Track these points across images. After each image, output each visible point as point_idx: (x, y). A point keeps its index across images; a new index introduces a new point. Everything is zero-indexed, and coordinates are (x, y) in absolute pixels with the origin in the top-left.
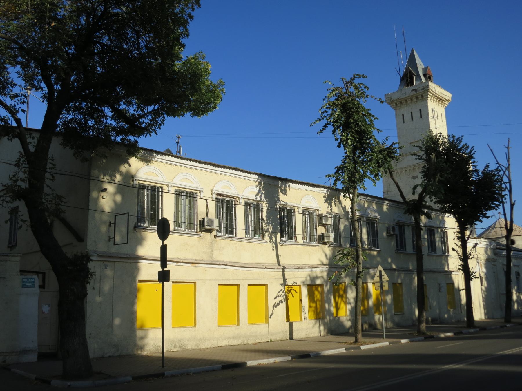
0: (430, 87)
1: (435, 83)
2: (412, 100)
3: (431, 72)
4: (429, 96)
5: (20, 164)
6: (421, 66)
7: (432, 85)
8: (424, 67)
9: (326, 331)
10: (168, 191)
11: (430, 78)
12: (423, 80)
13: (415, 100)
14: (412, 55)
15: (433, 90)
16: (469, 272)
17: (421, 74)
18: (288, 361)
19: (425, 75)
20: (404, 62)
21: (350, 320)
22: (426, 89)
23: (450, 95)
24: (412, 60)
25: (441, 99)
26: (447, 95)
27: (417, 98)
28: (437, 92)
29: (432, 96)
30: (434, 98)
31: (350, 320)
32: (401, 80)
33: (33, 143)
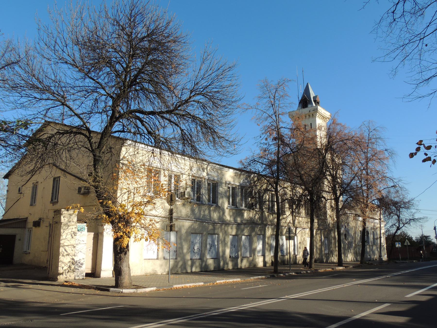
0: (319, 110)
1: (321, 107)
2: (306, 117)
3: (318, 99)
4: (317, 115)
5: (244, 169)
6: (312, 95)
7: (319, 108)
8: (314, 96)
9: (127, 277)
10: (387, 186)
11: (318, 103)
12: (314, 105)
13: (308, 117)
14: (307, 87)
15: (320, 111)
16: (279, 225)
17: (312, 100)
18: (249, 246)
19: (315, 101)
20: (302, 91)
21: (387, 197)
22: (316, 110)
23: (329, 114)
24: (307, 90)
25: (324, 117)
26: (327, 114)
27: (309, 116)
28: (322, 113)
29: (319, 115)
30: (320, 116)
31: (387, 197)
32: (299, 103)
33: (95, 139)
